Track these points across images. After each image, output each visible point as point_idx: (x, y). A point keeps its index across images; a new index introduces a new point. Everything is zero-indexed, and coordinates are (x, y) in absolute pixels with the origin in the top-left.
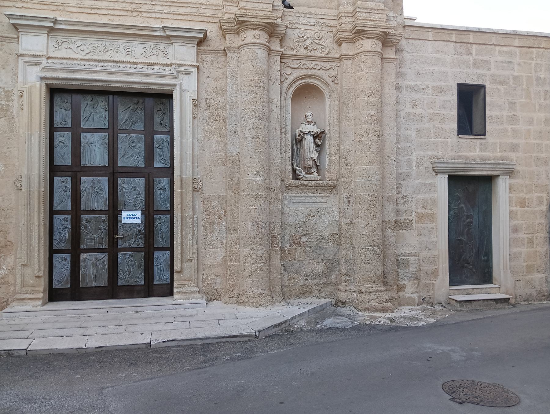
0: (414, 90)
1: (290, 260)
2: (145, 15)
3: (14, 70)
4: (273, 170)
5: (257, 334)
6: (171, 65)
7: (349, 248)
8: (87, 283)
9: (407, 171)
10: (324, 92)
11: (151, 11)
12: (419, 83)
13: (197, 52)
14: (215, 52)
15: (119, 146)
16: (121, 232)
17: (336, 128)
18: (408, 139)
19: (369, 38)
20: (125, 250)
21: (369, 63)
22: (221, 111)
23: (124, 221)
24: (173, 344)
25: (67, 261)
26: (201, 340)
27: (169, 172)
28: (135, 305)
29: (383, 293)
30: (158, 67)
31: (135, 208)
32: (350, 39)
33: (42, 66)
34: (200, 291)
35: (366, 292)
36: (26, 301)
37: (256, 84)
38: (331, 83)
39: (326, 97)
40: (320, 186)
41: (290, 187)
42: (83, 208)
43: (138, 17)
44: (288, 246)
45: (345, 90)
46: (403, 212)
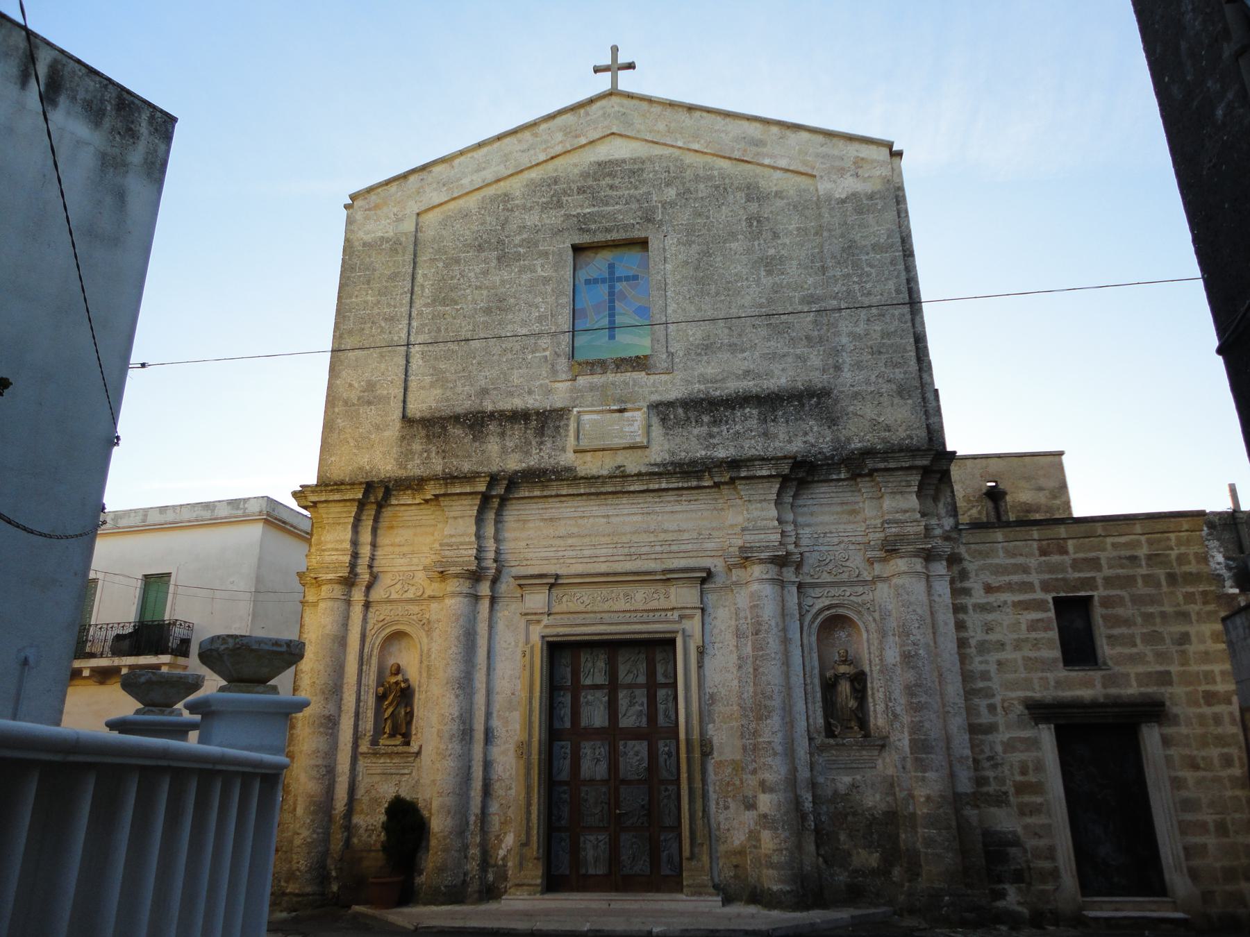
2: (643, 557)
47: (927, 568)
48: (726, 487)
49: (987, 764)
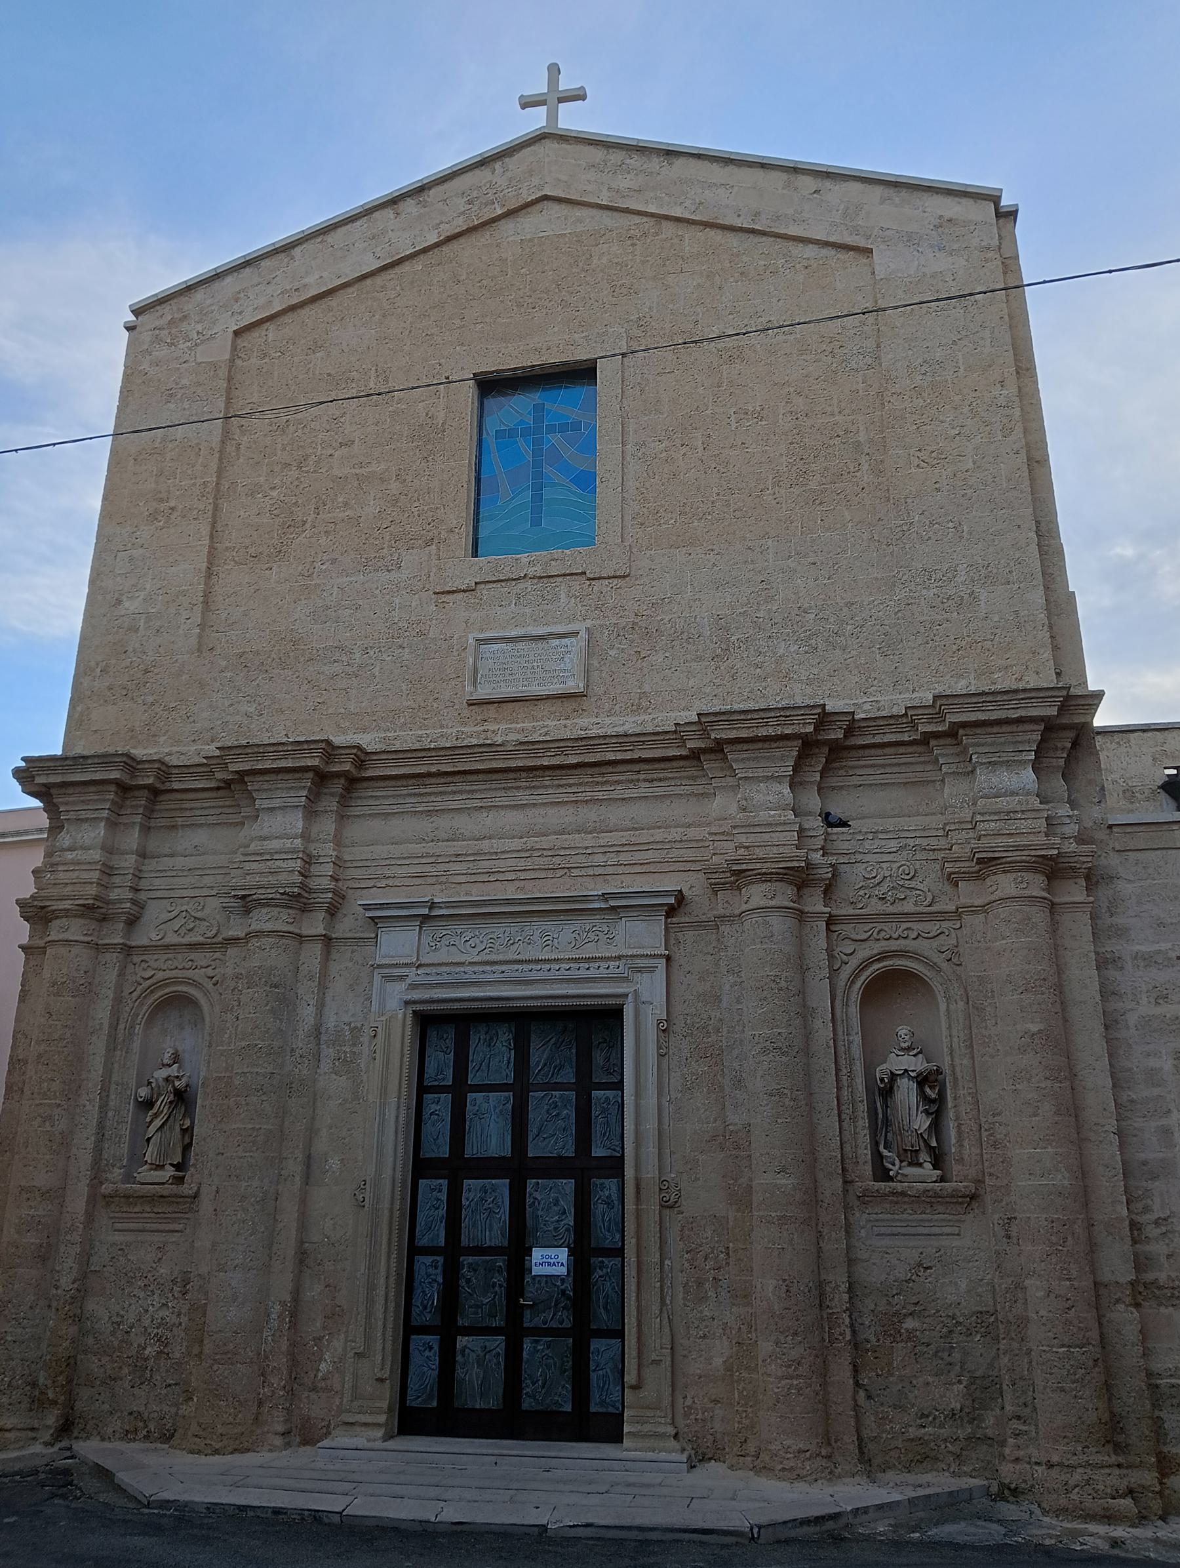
0: (1155, 962)
1: (878, 1375)
2: (576, 872)
3: (367, 991)
4: (823, 1161)
5: (756, 1530)
6: (619, 958)
7: (1019, 1350)
8: (466, 1400)
9: (1161, 1155)
10: (931, 983)
11: (586, 865)
12: (1164, 946)
13: (666, 929)
14: (700, 925)
15: (531, 1116)
16: (530, 1290)
17: (965, 1062)
18: (1153, 1078)
19: (1009, 871)
20: (537, 1332)
21: (1014, 923)
22: (714, 1037)
23: (536, 1271)
24: (589, 1532)
25: (433, 1351)
26: (640, 1531)
27: (615, 1166)
28: (546, 1454)
29: (1107, 1471)
30: (597, 964)
31: (556, 1243)
32: (973, 873)
33: (409, 981)
34: (680, 1435)
35: (1060, 1464)
36: (358, 1429)
37: (773, 985)
38: (945, 966)
39: (937, 992)
40: (937, 1195)
41: (867, 1199)
42: (464, 1241)
43: (565, 877)
44: (873, 1339)
45: (975, 979)
46: (1163, 1259)
47: (1048, 890)
48: (708, 756)
49: (1153, 1232)
